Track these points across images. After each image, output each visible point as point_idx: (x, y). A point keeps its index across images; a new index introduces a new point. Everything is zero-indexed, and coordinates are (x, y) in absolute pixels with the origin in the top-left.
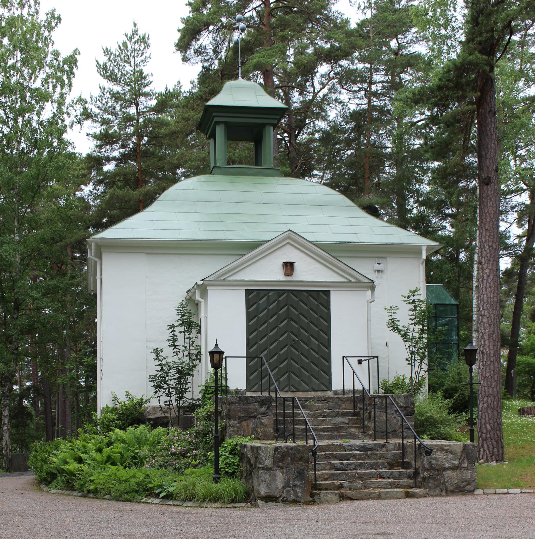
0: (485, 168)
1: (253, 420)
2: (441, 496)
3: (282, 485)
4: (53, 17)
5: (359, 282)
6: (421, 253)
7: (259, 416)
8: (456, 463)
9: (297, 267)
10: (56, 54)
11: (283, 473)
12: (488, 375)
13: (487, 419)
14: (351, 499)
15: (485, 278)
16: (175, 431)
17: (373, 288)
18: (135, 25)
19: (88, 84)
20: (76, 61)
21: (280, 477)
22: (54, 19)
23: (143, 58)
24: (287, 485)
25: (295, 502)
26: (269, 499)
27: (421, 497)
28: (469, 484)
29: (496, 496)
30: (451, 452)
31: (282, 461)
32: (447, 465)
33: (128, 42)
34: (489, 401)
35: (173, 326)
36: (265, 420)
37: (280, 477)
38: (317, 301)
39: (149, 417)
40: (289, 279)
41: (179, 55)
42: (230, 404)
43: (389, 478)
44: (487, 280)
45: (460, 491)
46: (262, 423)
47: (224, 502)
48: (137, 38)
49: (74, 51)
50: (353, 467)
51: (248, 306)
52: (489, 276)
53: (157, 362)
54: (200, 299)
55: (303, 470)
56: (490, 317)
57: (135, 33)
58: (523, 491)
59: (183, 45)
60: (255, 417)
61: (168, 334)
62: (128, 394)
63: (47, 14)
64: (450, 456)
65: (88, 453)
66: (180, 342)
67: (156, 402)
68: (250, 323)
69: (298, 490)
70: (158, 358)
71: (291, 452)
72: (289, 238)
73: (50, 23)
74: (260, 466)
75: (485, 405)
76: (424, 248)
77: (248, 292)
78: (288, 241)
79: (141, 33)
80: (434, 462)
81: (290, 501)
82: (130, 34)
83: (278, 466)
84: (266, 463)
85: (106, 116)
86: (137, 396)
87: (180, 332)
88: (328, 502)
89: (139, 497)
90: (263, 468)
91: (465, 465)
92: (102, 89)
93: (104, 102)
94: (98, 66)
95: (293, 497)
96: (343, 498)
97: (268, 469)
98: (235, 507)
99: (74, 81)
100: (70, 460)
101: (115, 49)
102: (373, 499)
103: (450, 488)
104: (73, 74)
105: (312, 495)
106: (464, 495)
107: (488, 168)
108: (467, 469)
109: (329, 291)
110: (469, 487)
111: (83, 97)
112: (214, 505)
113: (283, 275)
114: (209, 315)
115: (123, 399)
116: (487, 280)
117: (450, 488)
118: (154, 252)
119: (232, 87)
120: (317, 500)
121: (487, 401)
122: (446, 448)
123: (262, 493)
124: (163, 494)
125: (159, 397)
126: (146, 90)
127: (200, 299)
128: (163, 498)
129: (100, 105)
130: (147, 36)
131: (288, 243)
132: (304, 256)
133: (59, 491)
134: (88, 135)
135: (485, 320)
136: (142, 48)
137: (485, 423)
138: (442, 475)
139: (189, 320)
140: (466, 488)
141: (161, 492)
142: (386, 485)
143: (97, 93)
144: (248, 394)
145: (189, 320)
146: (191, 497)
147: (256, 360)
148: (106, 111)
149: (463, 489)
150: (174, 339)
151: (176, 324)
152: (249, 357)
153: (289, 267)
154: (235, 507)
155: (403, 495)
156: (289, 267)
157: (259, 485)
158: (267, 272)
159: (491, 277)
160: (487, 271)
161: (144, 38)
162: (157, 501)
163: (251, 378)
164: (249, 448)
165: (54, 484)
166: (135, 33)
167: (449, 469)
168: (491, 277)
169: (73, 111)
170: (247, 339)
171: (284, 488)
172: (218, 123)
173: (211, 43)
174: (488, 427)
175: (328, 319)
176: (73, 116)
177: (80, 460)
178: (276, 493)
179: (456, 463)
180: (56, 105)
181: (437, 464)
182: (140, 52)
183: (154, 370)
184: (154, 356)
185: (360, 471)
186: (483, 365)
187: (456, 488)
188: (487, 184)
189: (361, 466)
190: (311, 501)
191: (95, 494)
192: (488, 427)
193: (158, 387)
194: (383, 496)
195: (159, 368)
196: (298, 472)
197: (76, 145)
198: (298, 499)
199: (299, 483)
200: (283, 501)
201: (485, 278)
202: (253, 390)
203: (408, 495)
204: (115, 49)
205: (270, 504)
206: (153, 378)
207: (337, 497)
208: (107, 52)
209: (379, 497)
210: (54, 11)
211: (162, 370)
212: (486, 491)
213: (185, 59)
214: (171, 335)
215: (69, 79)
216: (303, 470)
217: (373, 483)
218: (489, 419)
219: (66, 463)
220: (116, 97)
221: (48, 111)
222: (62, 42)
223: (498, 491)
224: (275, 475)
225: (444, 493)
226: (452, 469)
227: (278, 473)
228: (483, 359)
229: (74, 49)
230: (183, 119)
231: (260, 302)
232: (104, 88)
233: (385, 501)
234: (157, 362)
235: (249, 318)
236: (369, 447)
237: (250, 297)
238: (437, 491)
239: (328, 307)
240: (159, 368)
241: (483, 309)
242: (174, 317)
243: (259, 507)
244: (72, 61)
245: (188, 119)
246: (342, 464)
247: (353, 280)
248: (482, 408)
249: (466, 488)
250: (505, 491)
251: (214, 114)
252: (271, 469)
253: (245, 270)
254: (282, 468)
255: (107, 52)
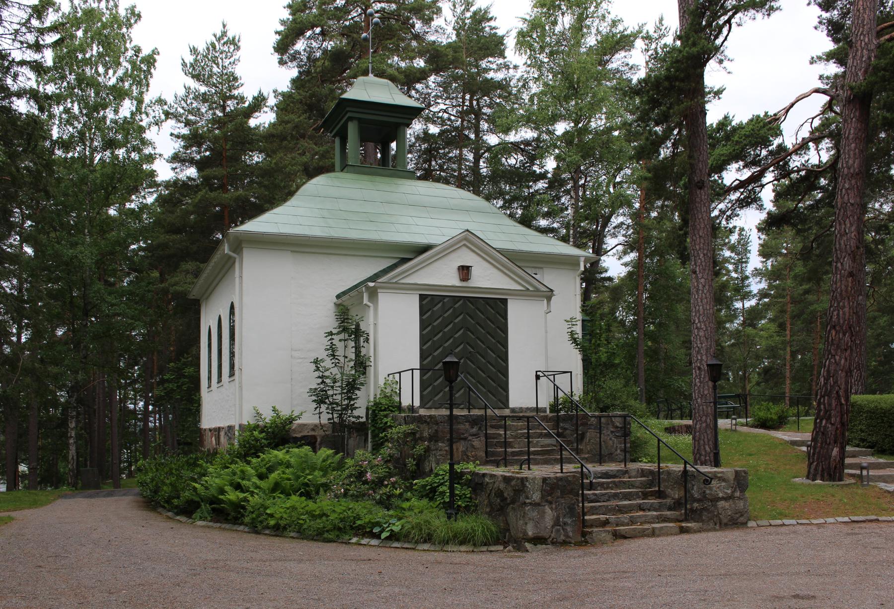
0: (698, 171)
1: (463, 442)
2: (715, 530)
3: (552, 524)
4: (133, 13)
5: (538, 290)
6: (579, 265)
7: (470, 438)
8: (729, 492)
9: (474, 272)
10: (138, 50)
11: (551, 509)
12: (706, 392)
13: (706, 440)
14: (625, 538)
15: (701, 288)
16: (325, 452)
17: (549, 299)
18: (224, 26)
19: (169, 83)
20: (155, 61)
21: (549, 513)
22: (135, 15)
23: (232, 60)
24: (557, 523)
25: (565, 543)
26: (538, 540)
27: (695, 532)
28: (742, 515)
29: (770, 529)
30: (724, 480)
31: (550, 495)
32: (721, 495)
33: (217, 43)
34: (708, 420)
35: (331, 334)
36: (476, 443)
37: (549, 513)
38: (491, 313)
39: (295, 435)
40: (464, 284)
41: (277, 56)
42: (437, 424)
43: (649, 510)
44: (703, 291)
45: (734, 524)
46: (473, 446)
47: (475, 545)
48: (226, 39)
49: (153, 51)
50: (606, 497)
51: (422, 313)
52: (704, 286)
53: (317, 374)
54: (369, 304)
55: (574, 504)
56: (707, 330)
57: (224, 34)
58: (800, 521)
59: (283, 47)
60: (465, 439)
61: (326, 342)
62: (274, 410)
63: (127, 10)
64: (723, 484)
65: (249, 480)
66: (340, 353)
67: (310, 416)
68: (424, 332)
69: (569, 529)
70: (318, 369)
71: (560, 483)
72: (466, 239)
73: (128, 20)
74: (528, 501)
75: (704, 425)
76: (582, 259)
77: (422, 297)
78: (465, 242)
79: (230, 35)
80: (708, 492)
81: (560, 543)
82: (219, 34)
83: (547, 501)
84: (534, 497)
85: (191, 117)
86: (285, 413)
87: (340, 340)
88: (603, 543)
89: (347, 537)
90: (530, 504)
91: (737, 494)
92: (187, 89)
93: (189, 102)
94: (184, 64)
95: (562, 537)
96: (618, 536)
97: (536, 505)
98: (491, 551)
99: (151, 81)
100: (227, 488)
101: (202, 48)
102: (648, 536)
103: (725, 521)
104: (151, 74)
105: (584, 534)
106: (738, 528)
107: (701, 171)
108: (739, 498)
109: (506, 299)
110: (742, 519)
111: (163, 98)
112: (463, 548)
113: (458, 279)
114: (381, 322)
115: (268, 416)
116: (703, 291)
117: (725, 521)
118: (313, 250)
119: (365, 83)
120: (589, 540)
121: (706, 421)
122: (719, 475)
123: (530, 533)
124: (384, 535)
125: (320, 413)
126: (235, 92)
127: (369, 304)
128: (387, 538)
129: (185, 105)
130: (237, 38)
131: (465, 245)
132: (481, 259)
133: (211, 524)
134: (172, 135)
135: (701, 333)
136: (231, 50)
137: (704, 445)
138: (715, 506)
139: (349, 325)
140: (739, 521)
141: (382, 532)
142: (653, 518)
143: (182, 92)
144: (423, 412)
145: (349, 325)
146: (428, 539)
147: (430, 373)
148: (190, 112)
149: (737, 522)
150: (332, 349)
151: (335, 331)
152: (423, 370)
153: (465, 272)
154: (491, 551)
155: (678, 530)
156: (465, 272)
157: (526, 524)
158: (441, 275)
159: (707, 287)
160: (702, 280)
161: (234, 39)
162: (374, 542)
163: (425, 393)
164: (500, 478)
165: (197, 515)
166: (224, 34)
167: (723, 499)
168: (707, 287)
169: (151, 112)
170: (421, 349)
171: (553, 527)
172: (351, 119)
173: (305, 50)
174: (707, 449)
175: (505, 330)
176: (151, 117)
177: (238, 487)
178: (546, 535)
179: (729, 492)
180: (135, 103)
181: (711, 494)
182: (229, 54)
183: (314, 383)
184: (313, 367)
185: (613, 503)
186: (700, 382)
187: (730, 521)
188: (700, 188)
189: (615, 496)
190: (582, 542)
191: (279, 530)
192: (707, 449)
193: (320, 402)
194: (657, 532)
195: (320, 380)
196: (569, 507)
197: (157, 145)
198: (568, 540)
199: (569, 521)
200: (553, 543)
201: (701, 288)
202: (427, 406)
203: (683, 531)
204: (202, 48)
205: (539, 546)
206: (313, 391)
207: (609, 537)
208: (194, 51)
209: (653, 534)
210: (135, 7)
211: (323, 382)
212: (759, 522)
213: (282, 62)
214: (329, 343)
215: (146, 78)
216: (574, 504)
217: (639, 517)
218: (709, 441)
219: (222, 491)
220: (204, 98)
221: (127, 108)
222: (141, 37)
223: (773, 522)
224: (544, 513)
225: (717, 527)
226: (725, 499)
227: (547, 509)
228: (700, 375)
229: (153, 48)
230: (283, 122)
231: (435, 309)
232: (190, 88)
233: (661, 538)
234: (317, 374)
235: (423, 325)
236: (611, 473)
237: (424, 303)
238: (711, 525)
239: (506, 318)
240: (320, 380)
241: (699, 322)
242: (330, 322)
243: (527, 551)
244: (150, 61)
245: (287, 122)
246: (595, 495)
247: (531, 289)
248: (700, 428)
249: (739, 521)
250: (779, 522)
251: (348, 109)
252: (538, 504)
253: (419, 273)
254: (551, 503)
255: (194, 51)
